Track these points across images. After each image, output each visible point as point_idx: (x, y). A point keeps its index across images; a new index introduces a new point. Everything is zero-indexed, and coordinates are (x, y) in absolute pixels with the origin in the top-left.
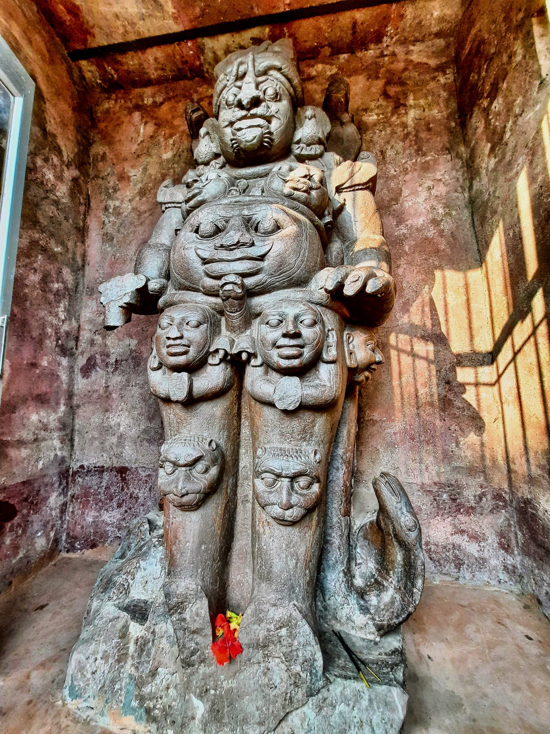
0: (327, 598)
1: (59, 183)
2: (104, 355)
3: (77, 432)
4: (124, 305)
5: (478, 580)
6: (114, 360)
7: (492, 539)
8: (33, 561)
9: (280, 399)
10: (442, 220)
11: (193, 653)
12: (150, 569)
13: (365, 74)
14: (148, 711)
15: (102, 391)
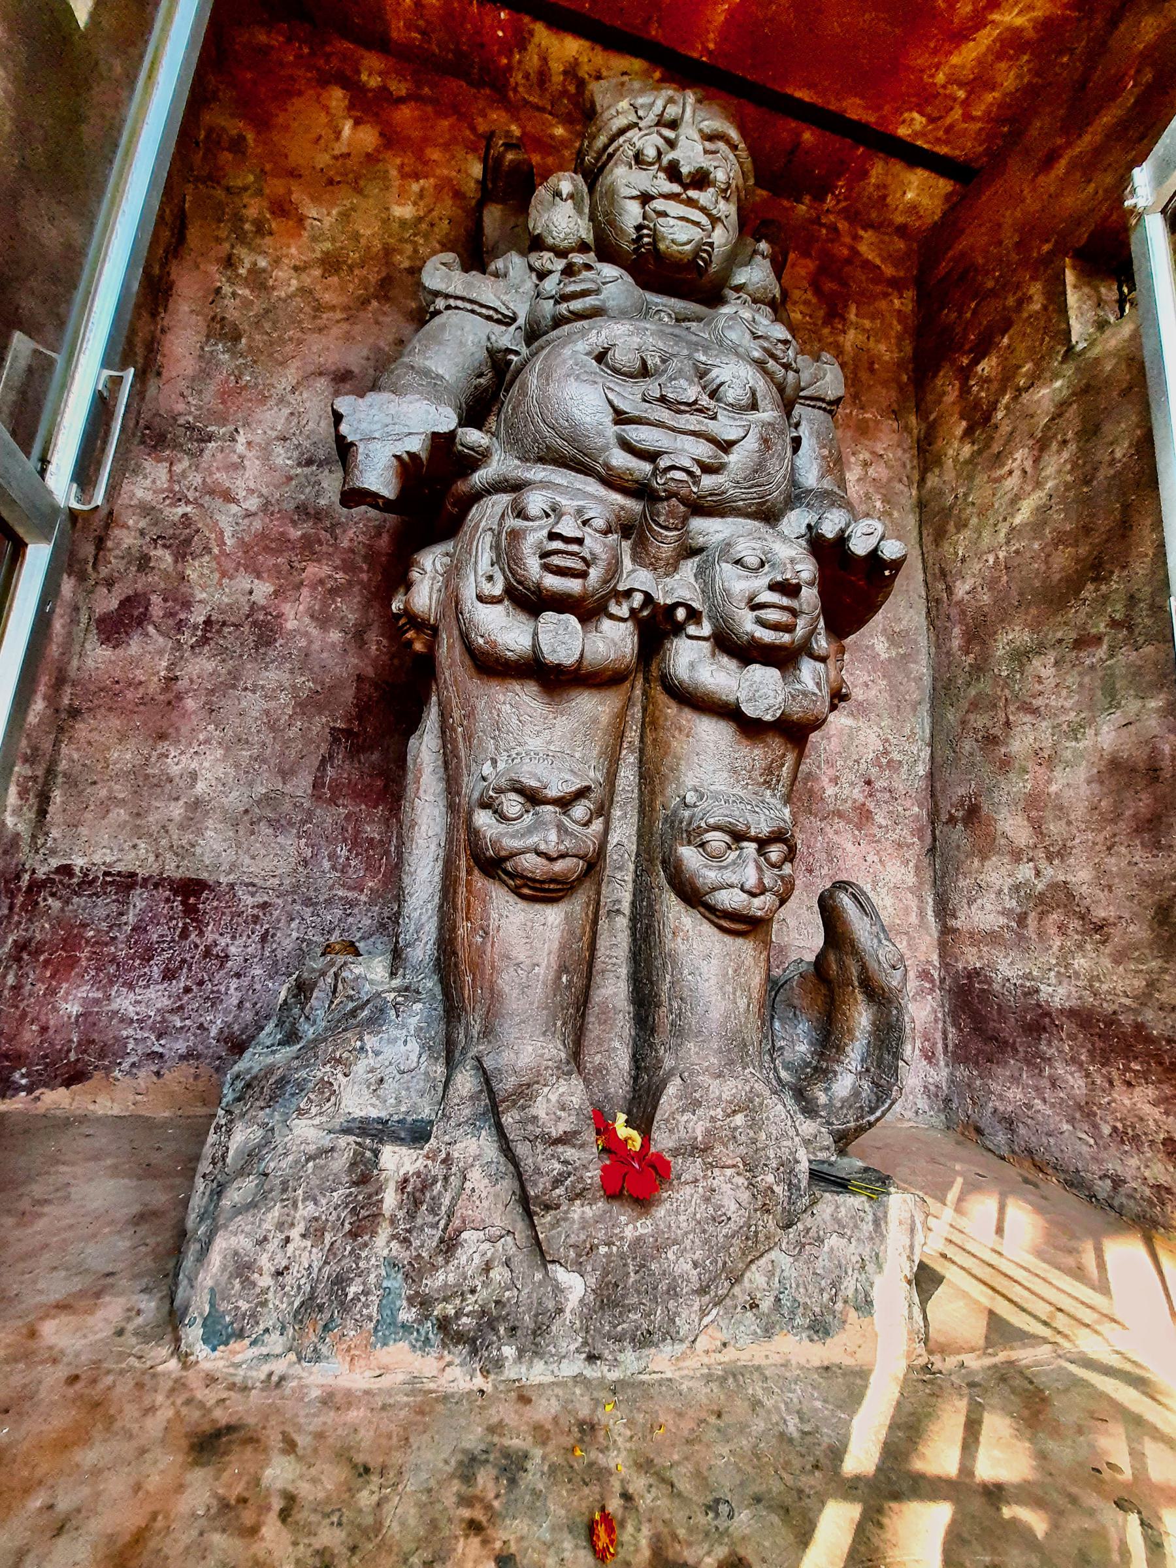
2: (175, 600)
3: (60, 780)
4: (405, 456)
6: (201, 619)
12: (389, 1052)
14: (443, 1324)
15: (154, 687)
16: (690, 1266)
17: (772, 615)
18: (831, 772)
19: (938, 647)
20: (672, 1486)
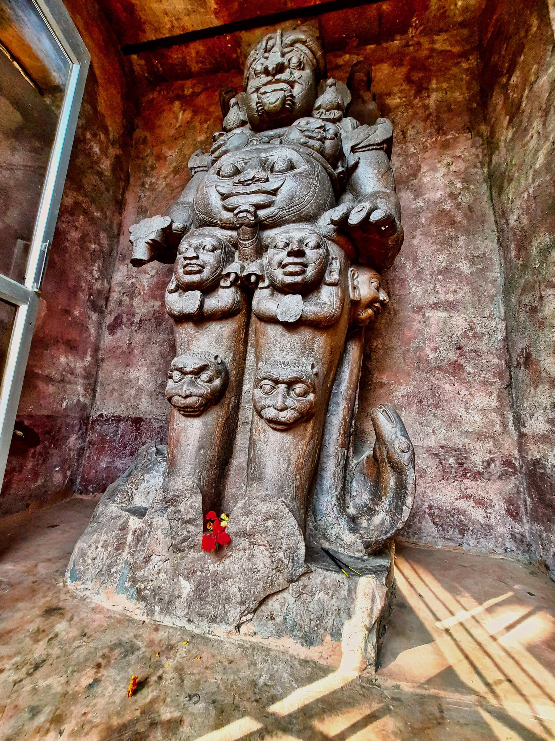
0: (318, 518)
1: (104, 158)
3: (99, 384)
4: (150, 242)
5: (483, 547)
7: (500, 506)
8: (49, 493)
9: (283, 313)
10: (460, 194)
11: (184, 540)
12: (153, 481)
13: (391, 61)
15: (125, 346)
16: (237, 590)
17: (290, 269)
18: (433, 345)
19: (505, 259)
20: (183, 681)
